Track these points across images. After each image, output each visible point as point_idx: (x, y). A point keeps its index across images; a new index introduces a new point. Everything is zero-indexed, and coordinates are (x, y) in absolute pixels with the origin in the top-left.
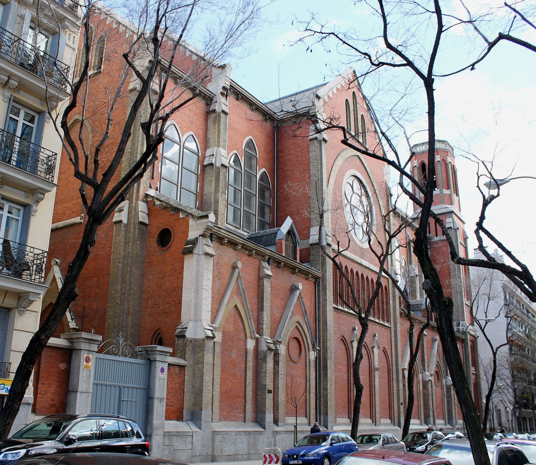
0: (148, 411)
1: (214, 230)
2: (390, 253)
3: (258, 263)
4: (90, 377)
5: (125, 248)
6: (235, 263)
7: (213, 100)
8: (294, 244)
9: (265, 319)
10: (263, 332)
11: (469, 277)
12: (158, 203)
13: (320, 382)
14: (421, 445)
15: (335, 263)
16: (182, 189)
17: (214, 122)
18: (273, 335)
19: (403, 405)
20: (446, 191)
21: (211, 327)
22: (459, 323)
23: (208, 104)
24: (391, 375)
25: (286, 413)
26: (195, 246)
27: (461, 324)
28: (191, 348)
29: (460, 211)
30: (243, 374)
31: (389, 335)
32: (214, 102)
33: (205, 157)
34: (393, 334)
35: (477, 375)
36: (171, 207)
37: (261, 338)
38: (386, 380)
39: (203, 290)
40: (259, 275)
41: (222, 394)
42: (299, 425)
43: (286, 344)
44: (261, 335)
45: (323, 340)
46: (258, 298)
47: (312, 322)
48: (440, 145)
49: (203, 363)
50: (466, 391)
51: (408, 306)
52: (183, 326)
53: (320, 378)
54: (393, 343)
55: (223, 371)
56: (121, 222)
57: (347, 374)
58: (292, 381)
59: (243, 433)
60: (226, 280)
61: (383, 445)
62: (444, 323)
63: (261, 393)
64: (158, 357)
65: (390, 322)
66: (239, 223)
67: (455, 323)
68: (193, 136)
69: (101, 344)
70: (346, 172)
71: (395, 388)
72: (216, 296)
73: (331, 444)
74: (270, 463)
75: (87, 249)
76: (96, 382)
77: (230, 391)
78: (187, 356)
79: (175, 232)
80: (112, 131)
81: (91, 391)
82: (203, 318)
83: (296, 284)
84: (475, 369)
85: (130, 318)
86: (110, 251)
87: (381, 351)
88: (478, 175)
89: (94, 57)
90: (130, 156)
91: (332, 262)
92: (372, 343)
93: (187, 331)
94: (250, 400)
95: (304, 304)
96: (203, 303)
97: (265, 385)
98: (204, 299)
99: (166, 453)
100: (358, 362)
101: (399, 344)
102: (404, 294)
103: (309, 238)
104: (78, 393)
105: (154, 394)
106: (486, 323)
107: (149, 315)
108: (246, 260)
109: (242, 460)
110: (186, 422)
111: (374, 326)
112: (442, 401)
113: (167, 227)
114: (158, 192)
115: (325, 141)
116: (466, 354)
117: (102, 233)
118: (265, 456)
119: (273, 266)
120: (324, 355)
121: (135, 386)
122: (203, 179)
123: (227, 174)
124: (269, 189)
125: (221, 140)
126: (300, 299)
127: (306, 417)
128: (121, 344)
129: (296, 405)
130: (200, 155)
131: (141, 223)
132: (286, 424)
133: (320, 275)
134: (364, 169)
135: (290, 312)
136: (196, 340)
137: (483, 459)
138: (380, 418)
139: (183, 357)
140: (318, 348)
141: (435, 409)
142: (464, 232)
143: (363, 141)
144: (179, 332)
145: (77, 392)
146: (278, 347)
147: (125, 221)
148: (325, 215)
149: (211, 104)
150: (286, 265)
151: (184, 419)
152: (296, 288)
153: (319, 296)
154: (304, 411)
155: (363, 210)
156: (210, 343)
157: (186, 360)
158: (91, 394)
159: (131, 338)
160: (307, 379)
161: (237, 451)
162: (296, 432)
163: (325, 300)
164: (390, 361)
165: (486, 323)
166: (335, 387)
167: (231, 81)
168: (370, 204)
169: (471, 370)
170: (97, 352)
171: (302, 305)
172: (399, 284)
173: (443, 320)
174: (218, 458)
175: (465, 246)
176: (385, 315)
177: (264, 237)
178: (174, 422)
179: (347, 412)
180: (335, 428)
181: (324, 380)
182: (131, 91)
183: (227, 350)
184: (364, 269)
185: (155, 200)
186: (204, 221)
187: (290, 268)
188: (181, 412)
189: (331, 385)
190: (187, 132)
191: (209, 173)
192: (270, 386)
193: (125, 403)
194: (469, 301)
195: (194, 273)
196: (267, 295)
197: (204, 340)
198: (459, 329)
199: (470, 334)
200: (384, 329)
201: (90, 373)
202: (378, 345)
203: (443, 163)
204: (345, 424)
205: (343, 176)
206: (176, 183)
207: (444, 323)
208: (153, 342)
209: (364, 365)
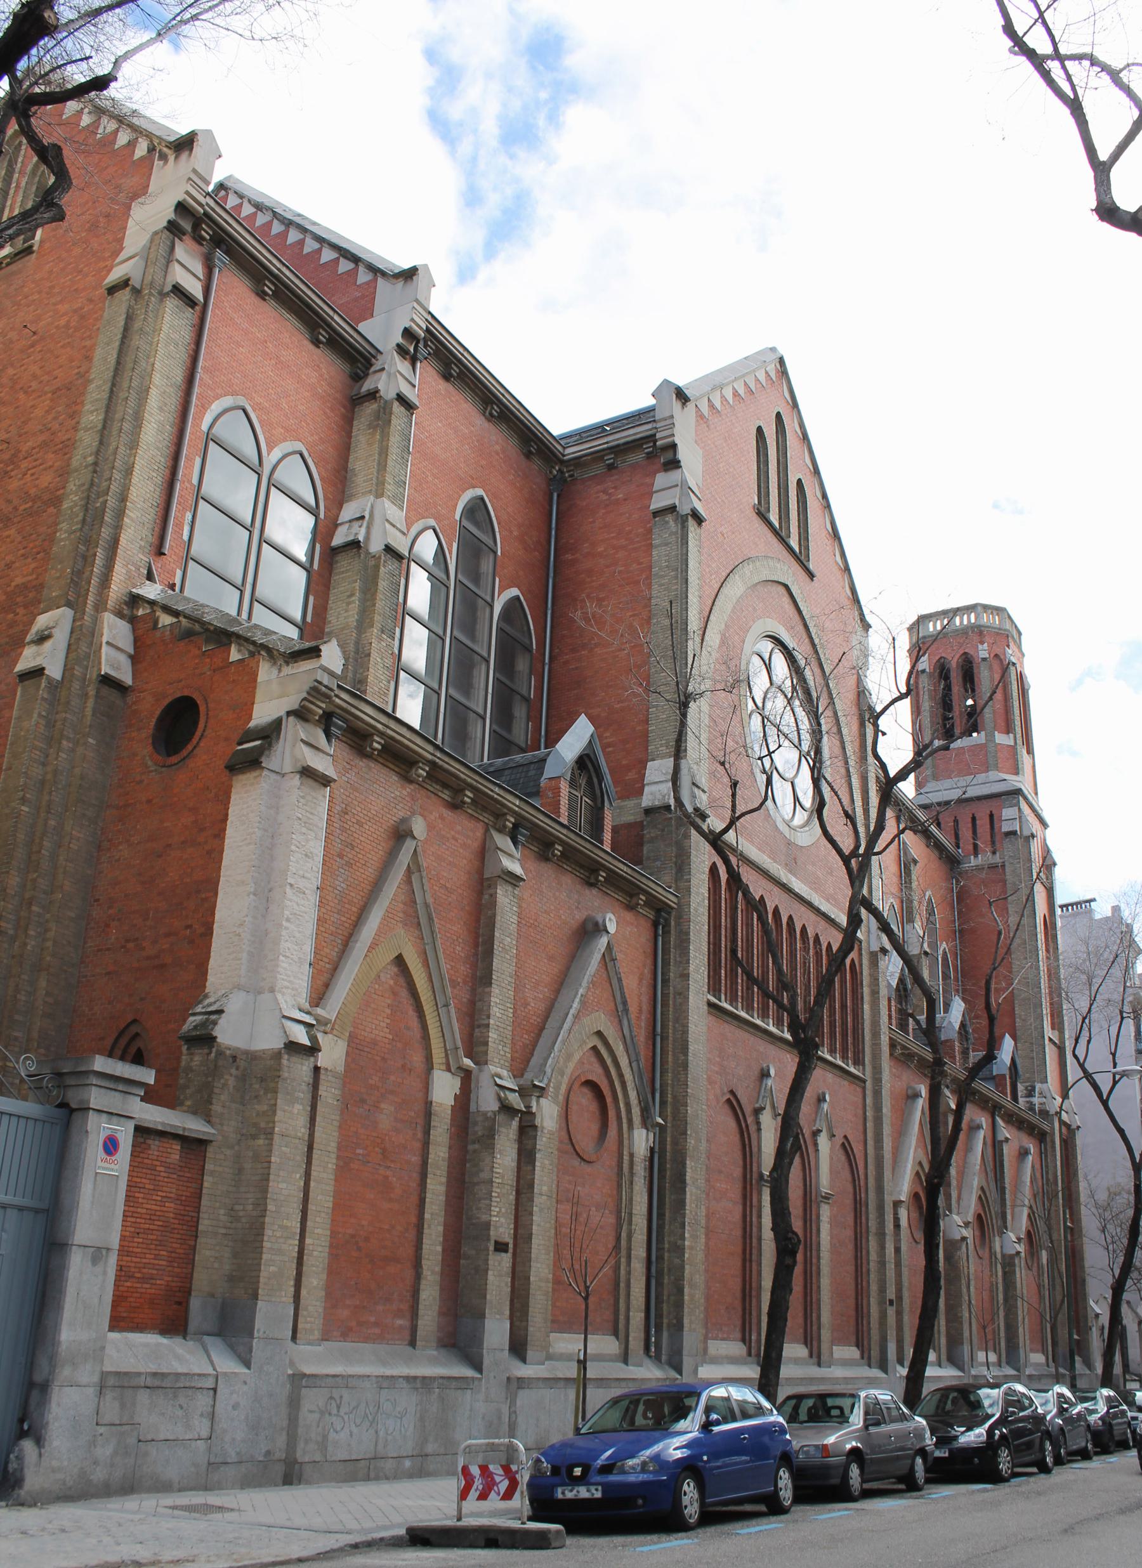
0: (44, 1295)
1: (337, 700)
3: (479, 834)
5: (47, 756)
6: (404, 820)
7: (371, 365)
8: (594, 799)
9: (495, 1011)
10: (486, 1053)
18: (519, 1066)
19: (894, 1308)
20: (1001, 739)
21: (308, 1013)
22: (1033, 1088)
23: (356, 374)
25: (553, 1321)
26: (270, 745)
27: (1037, 1090)
28: (232, 1082)
29: (1036, 794)
31: (860, 1101)
34: (869, 1101)
36: (207, 630)
37: (481, 1071)
39: (288, 889)
40: (480, 871)
41: (338, 1248)
42: (593, 1360)
43: (561, 1098)
44: (481, 1061)
45: (674, 1097)
46: (476, 945)
49: (269, 1134)
52: (210, 1005)
53: (661, 1216)
54: (870, 1125)
55: (344, 1169)
57: (741, 1207)
58: (575, 1216)
59: (404, 1384)
60: (370, 872)
61: (866, 1427)
63: (473, 1252)
64: (97, 1098)
65: (864, 1065)
68: (302, 455)
73: (706, 1426)
74: (483, 1496)
77: (367, 1239)
78: (216, 1108)
79: (211, 705)
80: (47, 412)
85: (43, 983)
87: (838, 1146)
90: (89, 477)
92: (815, 1121)
93: (223, 1021)
94: (433, 1272)
95: (620, 980)
96: (284, 933)
97: (487, 1225)
98: (288, 920)
99: (104, 1452)
100: (787, 1161)
103: (640, 792)
106: (1115, 1083)
107: (108, 973)
108: (442, 818)
113: (186, 693)
115: (699, 519)
118: (465, 1470)
119: (527, 852)
120: (675, 1143)
122: (327, 586)
124: (528, 649)
125: (389, 478)
126: (610, 965)
127: (616, 1333)
129: (587, 1288)
130: (322, 516)
131: (107, 681)
132: (550, 1357)
133: (671, 900)
135: (577, 1000)
136: (253, 1057)
138: (833, 1343)
139: (203, 1110)
140: (660, 1120)
144: (195, 1027)
146: (534, 1104)
147: (55, 671)
149: (366, 375)
151: (193, 1325)
152: (598, 929)
153: (666, 963)
156: (299, 1070)
157: (214, 1120)
159: (42, 1051)
160: (622, 1218)
161: (380, 1447)
162: (582, 1383)
163: (685, 976)
164: (862, 1177)
165: (1115, 1083)
166: (707, 1244)
171: (615, 982)
175: (1048, 885)
177: (506, 772)
178: (151, 1339)
179: (739, 1323)
182: (112, 290)
183: (363, 1101)
187: (582, 866)
188: (179, 1303)
189: (694, 1237)
190: (285, 440)
191: (347, 571)
192: (502, 1227)
194: (1056, 1032)
196: (506, 938)
197: (277, 1055)
198: (1031, 1103)
200: (846, 1083)
206: (239, 582)
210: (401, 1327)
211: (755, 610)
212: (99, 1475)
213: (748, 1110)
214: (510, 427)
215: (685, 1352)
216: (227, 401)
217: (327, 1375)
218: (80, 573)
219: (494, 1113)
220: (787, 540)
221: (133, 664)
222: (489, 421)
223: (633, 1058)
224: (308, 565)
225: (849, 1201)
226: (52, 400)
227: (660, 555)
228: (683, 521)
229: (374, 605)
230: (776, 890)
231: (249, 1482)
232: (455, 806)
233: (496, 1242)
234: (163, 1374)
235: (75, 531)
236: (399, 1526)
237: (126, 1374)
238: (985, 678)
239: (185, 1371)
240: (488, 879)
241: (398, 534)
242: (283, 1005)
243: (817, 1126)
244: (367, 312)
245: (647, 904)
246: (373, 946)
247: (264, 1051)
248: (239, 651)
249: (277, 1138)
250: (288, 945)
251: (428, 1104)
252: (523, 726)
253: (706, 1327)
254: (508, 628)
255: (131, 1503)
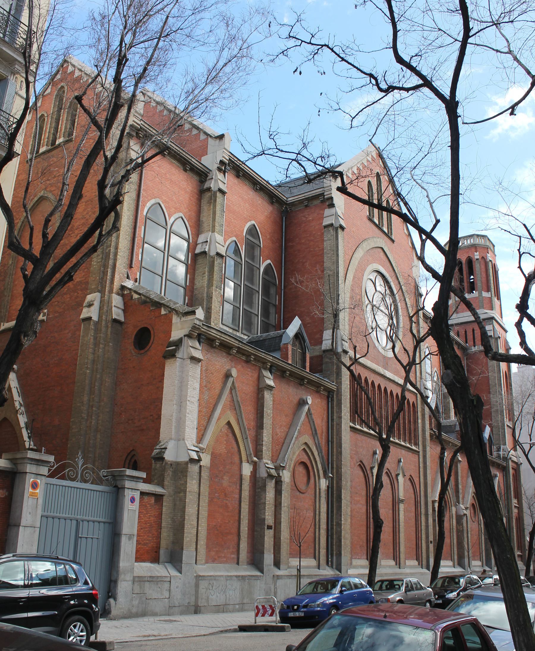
2: (417, 361)
4: (37, 507)
5: (95, 351)
6: (229, 370)
8: (302, 349)
9: (265, 439)
10: (262, 455)
11: (511, 394)
12: (136, 296)
13: (332, 516)
14: (452, 592)
15: (351, 372)
16: (167, 281)
17: (209, 203)
20: (485, 294)
21: (197, 447)
23: (202, 181)
24: (419, 508)
25: (290, 554)
26: (179, 349)
28: (171, 473)
29: (502, 317)
30: (237, 506)
32: (209, 179)
33: (197, 245)
35: (520, 508)
36: (152, 301)
37: (260, 462)
38: (413, 514)
40: (258, 385)
43: (291, 469)
44: (260, 457)
45: (337, 465)
46: (257, 414)
47: (323, 443)
48: (479, 241)
49: (185, 492)
50: (499, 523)
51: (439, 426)
52: (162, 445)
53: (332, 512)
54: (422, 470)
55: (211, 501)
56: (90, 319)
59: (235, 578)
60: (217, 391)
62: (470, 429)
64: (128, 484)
66: (237, 324)
67: (495, 448)
68: (182, 218)
69: (53, 466)
70: (368, 266)
71: (423, 523)
72: (204, 410)
73: (341, 592)
74: (263, 615)
75: (19, 340)
76: (46, 514)
77: (220, 527)
78: (166, 483)
81: (38, 525)
82: (186, 437)
83: (304, 397)
84: (518, 501)
85: (99, 436)
86: (77, 354)
88: (520, 252)
89: (65, 122)
91: (348, 373)
92: (397, 470)
95: (313, 422)
98: (188, 413)
99: (136, 602)
100: (378, 492)
101: (429, 471)
102: (435, 413)
103: (321, 343)
104: (21, 527)
105: (120, 529)
106: (531, 447)
107: (122, 432)
109: (233, 611)
110: (164, 564)
111: (399, 450)
112: (479, 538)
113: (145, 326)
114: (137, 284)
115: (342, 228)
116: (507, 484)
117: (68, 333)
118: (257, 607)
121: (98, 519)
123: (224, 265)
124: (275, 284)
125: (217, 224)
127: (315, 558)
128: (80, 466)
130: (191, 241)
131: (115, 321)
132: (289, 567)
133: (334, 388)
134: (389, 264)
136: (178, 464)
137: (521, 619)
138: (405, 559)
139: (161, 484)
140: (331, 475)
141: (470, 548)
142: (506, 342)
143: (388, 231)
144: (157, 454)
145: (18, 526)
146: (281, 473)
147: (95, 318)
148: (341, 315)
149: (206, 181)
150: (293, 375)
154: (312, 551)
155: (387, 313)
156: (194, 469)
157: (165, 487)
158: (38, 530)
159: (100, 461)
162: (299, 576)
163: (340, 418)
165: (531, 447)
166: (351, 522)
167: (230, 155)
168: (394, 301)
169: (513, 503)
170: (48, 477)
172: (429, 401)
173: (469, 425)
174: (202, 608)
176: (413, 437)
180: (350, 572)
181: (337, 514)
184: (388, 382)
185: (133, 293)
186: (190, 317)
187: (298, 378)
188: (156, 552)
191: (202, 263)
193: (84, 540)
194: (511, 422)
195: (176, 382)
197: (187, 463)
199: (513, 461)
200: (410, 453)
201: (37, 503)
202: (403, 473)
203: (482, 262)
204: (362, 567)
205: (364, 270)
207: (470, 429)
208: (127, 466)
209: (385, 494)
210: (233, 558)
211: (368, 261)
212: (134, 610)
213: (368, 468)
214: (264, 193)
215: (342, 564)
216: (153, 201)
217: (208, 576)
218: (102, 278)
219: (266, 477)
220: (382, 228)
221: (124, 313)
222: (256, 191)
223: (320, 451)
224: (186, 262)
225: (413, 502)
226: (85, 205)
227: (327, 245)
228: (337, 229)
229: (213, 277)
230: (378, 377)
231: (182, 613)
232: (248, 362)
233: (268, 526)
234: (153, 577)
235: (99, 262)
236: (236, 625)
237: (141, 577)
238: (477, 267)
239: (160, 575)
240: (261, 388)
241: (221, 247)
242: (188, 445)
243: (398, 472)
244: (204, 152)
245: (324, 390)
246: (219, 419)
247: (181, 462)
248: (165, 310)
249: (187, 493)
250: (189, 422)
251: (241, 475)
252: (274, 316)
253: (351, 553)
254: (266, 277)
255: (146, 619)
